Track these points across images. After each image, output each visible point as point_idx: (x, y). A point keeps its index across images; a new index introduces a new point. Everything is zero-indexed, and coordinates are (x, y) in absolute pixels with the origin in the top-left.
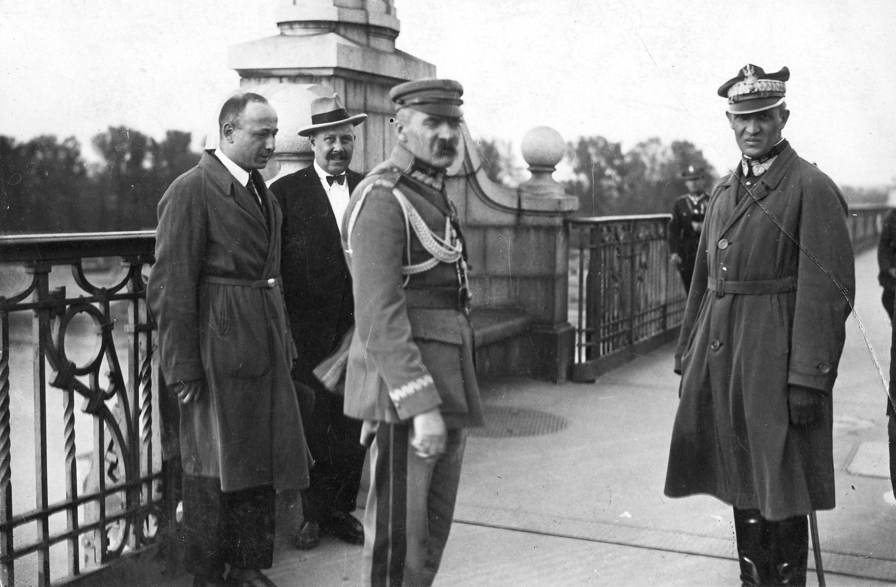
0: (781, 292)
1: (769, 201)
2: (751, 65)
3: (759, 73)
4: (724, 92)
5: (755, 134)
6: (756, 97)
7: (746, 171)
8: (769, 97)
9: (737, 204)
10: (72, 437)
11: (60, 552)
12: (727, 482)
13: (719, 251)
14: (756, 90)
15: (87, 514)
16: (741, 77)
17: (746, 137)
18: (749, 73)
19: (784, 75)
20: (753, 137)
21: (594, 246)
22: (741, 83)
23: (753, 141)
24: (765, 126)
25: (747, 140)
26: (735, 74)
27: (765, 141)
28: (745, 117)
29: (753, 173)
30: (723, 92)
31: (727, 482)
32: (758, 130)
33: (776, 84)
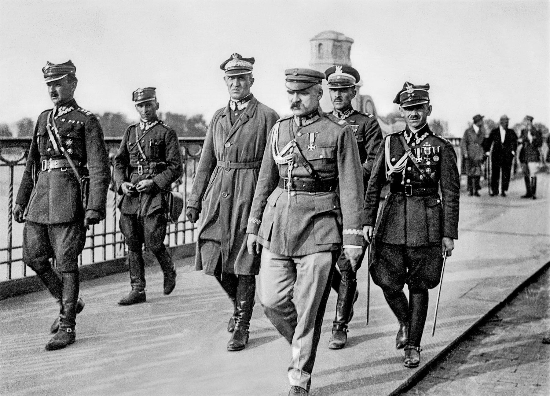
0: (254, 168)
1: (248, 124)
2: (236, 54)
3: (239, 57)
4: (223, 67)
5: (237, 86)
6: (239, 69)
7: (233, 107)
8: (244, 69)
9: (232, 125)
10: (11, 230)
11: (109, 248)
12: (47, 367)
13: (225, 149)
14: (238, 65)
15: (109, 239)
16: (231, 59)
17: (233, 88)
18: (234, 57)
19: (252, 61)
20: (236, 88)
21: (286, 178)
22: (231, 61)
23: (236, 90)
24: (242, 83)
25: (233, 90)
26: (229, 57)
27: (242, 91)
28: (233, 77)
29: (238, 109)
30: (223, 67)
31: (47, 367)
32: (238, 85)
33: (249, 64)
